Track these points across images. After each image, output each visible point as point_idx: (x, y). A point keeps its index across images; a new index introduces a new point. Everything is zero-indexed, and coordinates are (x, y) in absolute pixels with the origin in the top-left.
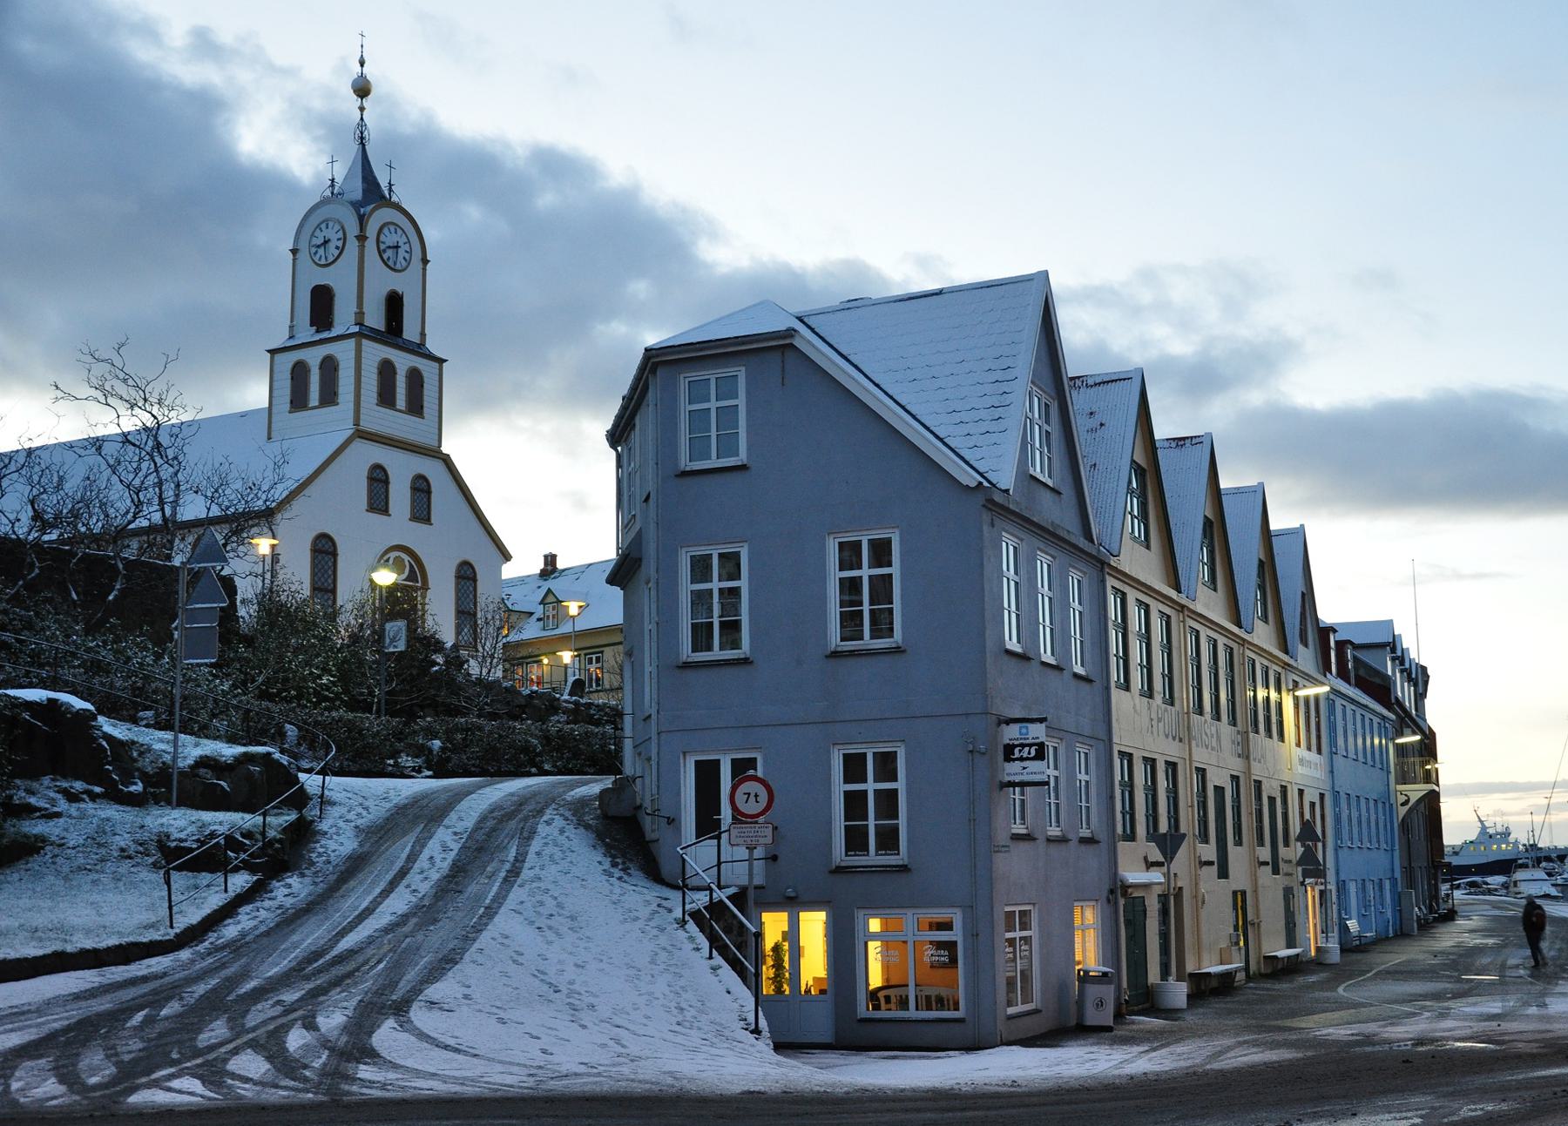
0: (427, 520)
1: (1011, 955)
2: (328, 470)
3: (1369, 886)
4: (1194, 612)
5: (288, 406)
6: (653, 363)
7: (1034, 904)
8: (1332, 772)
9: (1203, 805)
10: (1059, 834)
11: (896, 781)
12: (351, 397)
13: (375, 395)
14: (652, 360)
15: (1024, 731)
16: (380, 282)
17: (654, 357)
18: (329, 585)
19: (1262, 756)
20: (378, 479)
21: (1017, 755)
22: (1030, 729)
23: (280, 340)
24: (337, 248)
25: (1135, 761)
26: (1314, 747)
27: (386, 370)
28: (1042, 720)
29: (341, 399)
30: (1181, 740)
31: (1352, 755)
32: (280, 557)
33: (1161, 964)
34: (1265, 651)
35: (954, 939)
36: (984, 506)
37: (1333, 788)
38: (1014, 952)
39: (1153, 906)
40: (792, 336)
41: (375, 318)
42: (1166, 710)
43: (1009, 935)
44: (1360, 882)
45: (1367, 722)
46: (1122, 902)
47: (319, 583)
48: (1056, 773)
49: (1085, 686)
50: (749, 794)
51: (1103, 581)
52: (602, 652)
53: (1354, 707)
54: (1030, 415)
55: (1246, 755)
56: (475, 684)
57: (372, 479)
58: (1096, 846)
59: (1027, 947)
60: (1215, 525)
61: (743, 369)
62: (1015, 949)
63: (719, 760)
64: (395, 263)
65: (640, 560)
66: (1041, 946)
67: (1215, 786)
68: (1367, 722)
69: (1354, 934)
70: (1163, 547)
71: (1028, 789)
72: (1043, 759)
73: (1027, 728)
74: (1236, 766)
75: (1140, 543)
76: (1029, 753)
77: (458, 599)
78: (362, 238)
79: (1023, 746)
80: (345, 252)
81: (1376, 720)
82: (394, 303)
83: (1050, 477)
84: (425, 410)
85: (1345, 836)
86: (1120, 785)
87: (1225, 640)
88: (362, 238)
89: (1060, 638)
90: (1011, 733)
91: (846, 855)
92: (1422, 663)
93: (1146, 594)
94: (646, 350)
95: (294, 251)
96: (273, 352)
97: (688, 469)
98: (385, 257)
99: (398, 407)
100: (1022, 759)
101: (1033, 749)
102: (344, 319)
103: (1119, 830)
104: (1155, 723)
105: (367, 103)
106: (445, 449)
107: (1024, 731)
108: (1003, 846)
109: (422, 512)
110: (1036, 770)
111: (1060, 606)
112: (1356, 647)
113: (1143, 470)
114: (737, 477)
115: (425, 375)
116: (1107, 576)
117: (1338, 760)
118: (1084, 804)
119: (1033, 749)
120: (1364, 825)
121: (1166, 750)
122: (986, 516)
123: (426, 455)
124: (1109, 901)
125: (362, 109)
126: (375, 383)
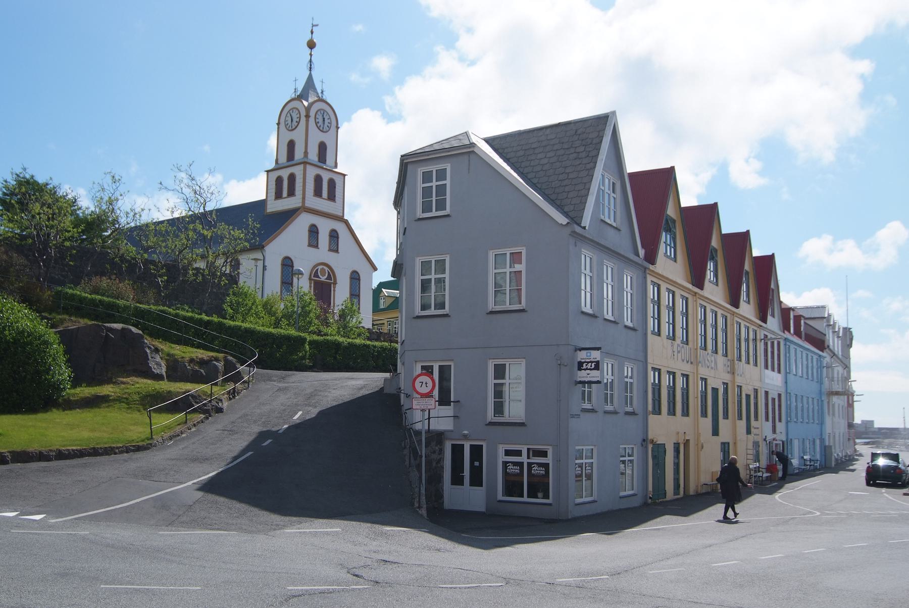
0: (337, 251)
1: (580, 472)
2: (353, 240)
3: (807, 443)
4: (703, 296)
5: (273, 198)
6: (406, 163)
7: (595, 446)
8: (786, 382)
9: (740, 402)
10: (612, 409)
13: (313, 191)
15: (589, 354)
16: (316, 137)
17: (405, 159)
18: (290, 281)
19: (743, 373)
20: (313, 231)
21: (585, 367)
25: (662, 373)
26: (776, 369)
27: (318, 180)
28: (598, 349)
30: (692, 363)
31: (800, 373)
32: (267, 267)
33: (674, 479)
34: (747, 318)
35: (547, 462)
36: (570, 235)
37: (787, 391)
40: (474, 147)
41: (313, 156)
42: (683, 347)
44: (801, 440)
45: (810, 358)
47: (285, 280)
48: (613, 378)
49: (631, 333)
50: (422, 383)
51: (645, 278)
53: (802, 350)
54: (602, 187)
55: (733, 372)
58: (595, 413)
59: (631, 465)
60: (718, 252)
61: (449, 165)
62: (582, 469)
63: (433, 366)
64: (323, 128)
65: (402, 264)
67: (713, 388)
69: (796, 467)
71: (594, 386)
73: (590, 353)
74: (727, 378)
75: (671, 259)
76: (591, 366)
77: (351, 288)
78: (307, 116)
79: (588, 362)
80: (317, 129)
81: (815, 357)
82: (322, 147)
83: (615, 221)
84: (337, 198)
85: (793, 415)
87: (723, 312)
88: (307, 116)
89: (618, 304)
90: (582, 356)
91: (494, 416)
93: (673, 285)
94: (402, 156)
95: (278, 124)
96: (268, 172)
97: (421, 217)
98: (319, 125)
99: (323, 197)
100: (587, 369)
102: (299, 155)
103: (650, 408)
104: (676, 354)
105: (314, 51)
106: (346, 218)
107: (589, 354)
108: (575, 415)
110: (594, 375)
111: (618, 290)
112: (806, 319)
114: (447, 219)
115: (336, 181)
116: (648, 275)
117: (791, 377)
119: (593, 364)
120: (805, 411)
121: (681, 367)
123: (336, 220)
124: (642, 445)
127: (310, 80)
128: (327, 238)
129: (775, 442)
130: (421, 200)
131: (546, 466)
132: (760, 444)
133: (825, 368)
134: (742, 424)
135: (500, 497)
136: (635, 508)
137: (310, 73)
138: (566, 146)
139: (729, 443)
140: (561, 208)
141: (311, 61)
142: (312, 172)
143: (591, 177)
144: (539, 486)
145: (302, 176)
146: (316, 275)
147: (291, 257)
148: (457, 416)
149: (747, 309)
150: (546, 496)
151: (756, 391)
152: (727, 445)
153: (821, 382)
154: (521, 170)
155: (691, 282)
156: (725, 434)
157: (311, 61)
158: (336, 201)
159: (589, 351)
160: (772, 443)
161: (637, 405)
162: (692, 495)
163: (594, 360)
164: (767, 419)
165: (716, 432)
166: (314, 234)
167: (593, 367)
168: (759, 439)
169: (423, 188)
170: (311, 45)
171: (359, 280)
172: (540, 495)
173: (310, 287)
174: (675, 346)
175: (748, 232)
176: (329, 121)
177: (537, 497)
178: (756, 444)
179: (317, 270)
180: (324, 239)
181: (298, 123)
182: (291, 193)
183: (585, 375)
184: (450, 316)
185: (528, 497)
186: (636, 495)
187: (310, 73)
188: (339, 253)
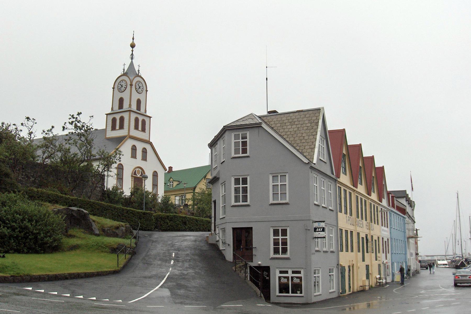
5: (111, 129)
8: (391, 233)
10: (326, 250)
11: (287, 236)
12: (128, 127)
14: (225, 129)
15: (319, 224)
16: (135, 96)
17: (226, 128)
21: (317, 230)
22: (321, 224)
23: (109, 111)
24: (125, 88)
27: (137, 120)
28: (324, 222)
29: (146, 130)
30: (354, 225)
36: (310, 168)
37: (391, 237)
38: (331, 278)
39: (347, 269)
41: (134, 107)
43: (315, 275)
46: (340, 267)
51: (336, 185)
52: (186, 195)
56: (122, 199)
57: (132, 149)
66: (322, 278)
68: (400, 218)
70: (327, 154)
72: (324, 232)
73: (320, 223)
76: (320, 230)
78: (131, 85)
79: (319, 228)
80: (127, 89)
81: (402, 218)
82: (139, 102)
84: (146, 130)
86: (340, 237)
88: (131, 85)
90: (316, 225)
91: (274, 255)
92: (413, 200)
95: (113, 88)
96: (107, 114)
99: (139, 130)
100: (319, 231)
101: (321, 229)
102: (126, 106)
104: (348, 221)
105: (134, 49)
107: (319, 224)
109: (144, 158)
110: (322, 234)
113: (345, 155)
115: (146, 121)
118: (324, 242)
119: (321, 229)
121: (350, 228)
122: (310, 170)
124: (337, 267)
125: (132, 51)
126: (134, 123)
127: (132, 65)
128: (141, 153)
129: (387, 264)
130: (234, 148)
131: (300, 278)
132: (381, 265)
133: (406, 224)
134: (374, 255)
135: (278, 294)
136: (335, 298)
137: (132, 61)
138: (301, 123)
139: (369, 265)
140: (302, 154)
141: (132, 54)
142: (133, 116)
143: (315, 139)
144: (297, 288)
145: (128, 118)
146: (135, 174)
147: (122, 164)
148: (255, 255)
149: (374, 196)
150: (301, 293)
151: (378, 238)
152: (368, 266)
153: (405, 232)
154: (280, 133)
155: (352, 185)
156: (367, 262)
157: (132, 54)
158: (146, 132)
159: (319, 223)
160: (386, 265)
161: (333, 249)
162: (355, 292)
163: (322, 227)
164: (383, 253)
165: (363, 260)
166: (134, 150)
167: (321, 230)
168: (381, 263)
169: (235, 142)
170: (133, 46)
171: (157, 176)
172: (298, 292)
173: (132, 180)
174: (348, 217)
175: (373, 156)
176: (142, 87)
177: (297, 293)
178: (379, 265)
179: (136, 170)
180: (139, 153)
181: (126, 88)
182: (121, 127)
183: (318, 234)
184: (250, 206)
185: (292, 293)
186: (321, 295)
187: (132, 61)
188: (147, 161)
